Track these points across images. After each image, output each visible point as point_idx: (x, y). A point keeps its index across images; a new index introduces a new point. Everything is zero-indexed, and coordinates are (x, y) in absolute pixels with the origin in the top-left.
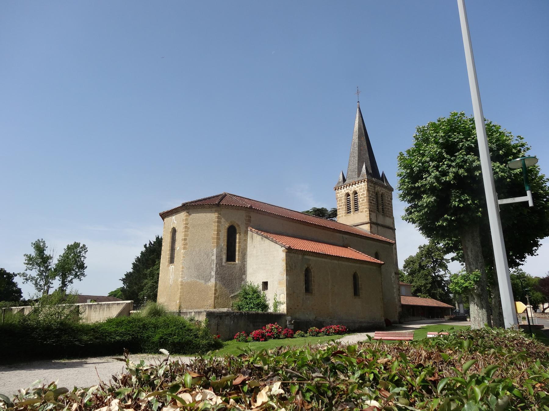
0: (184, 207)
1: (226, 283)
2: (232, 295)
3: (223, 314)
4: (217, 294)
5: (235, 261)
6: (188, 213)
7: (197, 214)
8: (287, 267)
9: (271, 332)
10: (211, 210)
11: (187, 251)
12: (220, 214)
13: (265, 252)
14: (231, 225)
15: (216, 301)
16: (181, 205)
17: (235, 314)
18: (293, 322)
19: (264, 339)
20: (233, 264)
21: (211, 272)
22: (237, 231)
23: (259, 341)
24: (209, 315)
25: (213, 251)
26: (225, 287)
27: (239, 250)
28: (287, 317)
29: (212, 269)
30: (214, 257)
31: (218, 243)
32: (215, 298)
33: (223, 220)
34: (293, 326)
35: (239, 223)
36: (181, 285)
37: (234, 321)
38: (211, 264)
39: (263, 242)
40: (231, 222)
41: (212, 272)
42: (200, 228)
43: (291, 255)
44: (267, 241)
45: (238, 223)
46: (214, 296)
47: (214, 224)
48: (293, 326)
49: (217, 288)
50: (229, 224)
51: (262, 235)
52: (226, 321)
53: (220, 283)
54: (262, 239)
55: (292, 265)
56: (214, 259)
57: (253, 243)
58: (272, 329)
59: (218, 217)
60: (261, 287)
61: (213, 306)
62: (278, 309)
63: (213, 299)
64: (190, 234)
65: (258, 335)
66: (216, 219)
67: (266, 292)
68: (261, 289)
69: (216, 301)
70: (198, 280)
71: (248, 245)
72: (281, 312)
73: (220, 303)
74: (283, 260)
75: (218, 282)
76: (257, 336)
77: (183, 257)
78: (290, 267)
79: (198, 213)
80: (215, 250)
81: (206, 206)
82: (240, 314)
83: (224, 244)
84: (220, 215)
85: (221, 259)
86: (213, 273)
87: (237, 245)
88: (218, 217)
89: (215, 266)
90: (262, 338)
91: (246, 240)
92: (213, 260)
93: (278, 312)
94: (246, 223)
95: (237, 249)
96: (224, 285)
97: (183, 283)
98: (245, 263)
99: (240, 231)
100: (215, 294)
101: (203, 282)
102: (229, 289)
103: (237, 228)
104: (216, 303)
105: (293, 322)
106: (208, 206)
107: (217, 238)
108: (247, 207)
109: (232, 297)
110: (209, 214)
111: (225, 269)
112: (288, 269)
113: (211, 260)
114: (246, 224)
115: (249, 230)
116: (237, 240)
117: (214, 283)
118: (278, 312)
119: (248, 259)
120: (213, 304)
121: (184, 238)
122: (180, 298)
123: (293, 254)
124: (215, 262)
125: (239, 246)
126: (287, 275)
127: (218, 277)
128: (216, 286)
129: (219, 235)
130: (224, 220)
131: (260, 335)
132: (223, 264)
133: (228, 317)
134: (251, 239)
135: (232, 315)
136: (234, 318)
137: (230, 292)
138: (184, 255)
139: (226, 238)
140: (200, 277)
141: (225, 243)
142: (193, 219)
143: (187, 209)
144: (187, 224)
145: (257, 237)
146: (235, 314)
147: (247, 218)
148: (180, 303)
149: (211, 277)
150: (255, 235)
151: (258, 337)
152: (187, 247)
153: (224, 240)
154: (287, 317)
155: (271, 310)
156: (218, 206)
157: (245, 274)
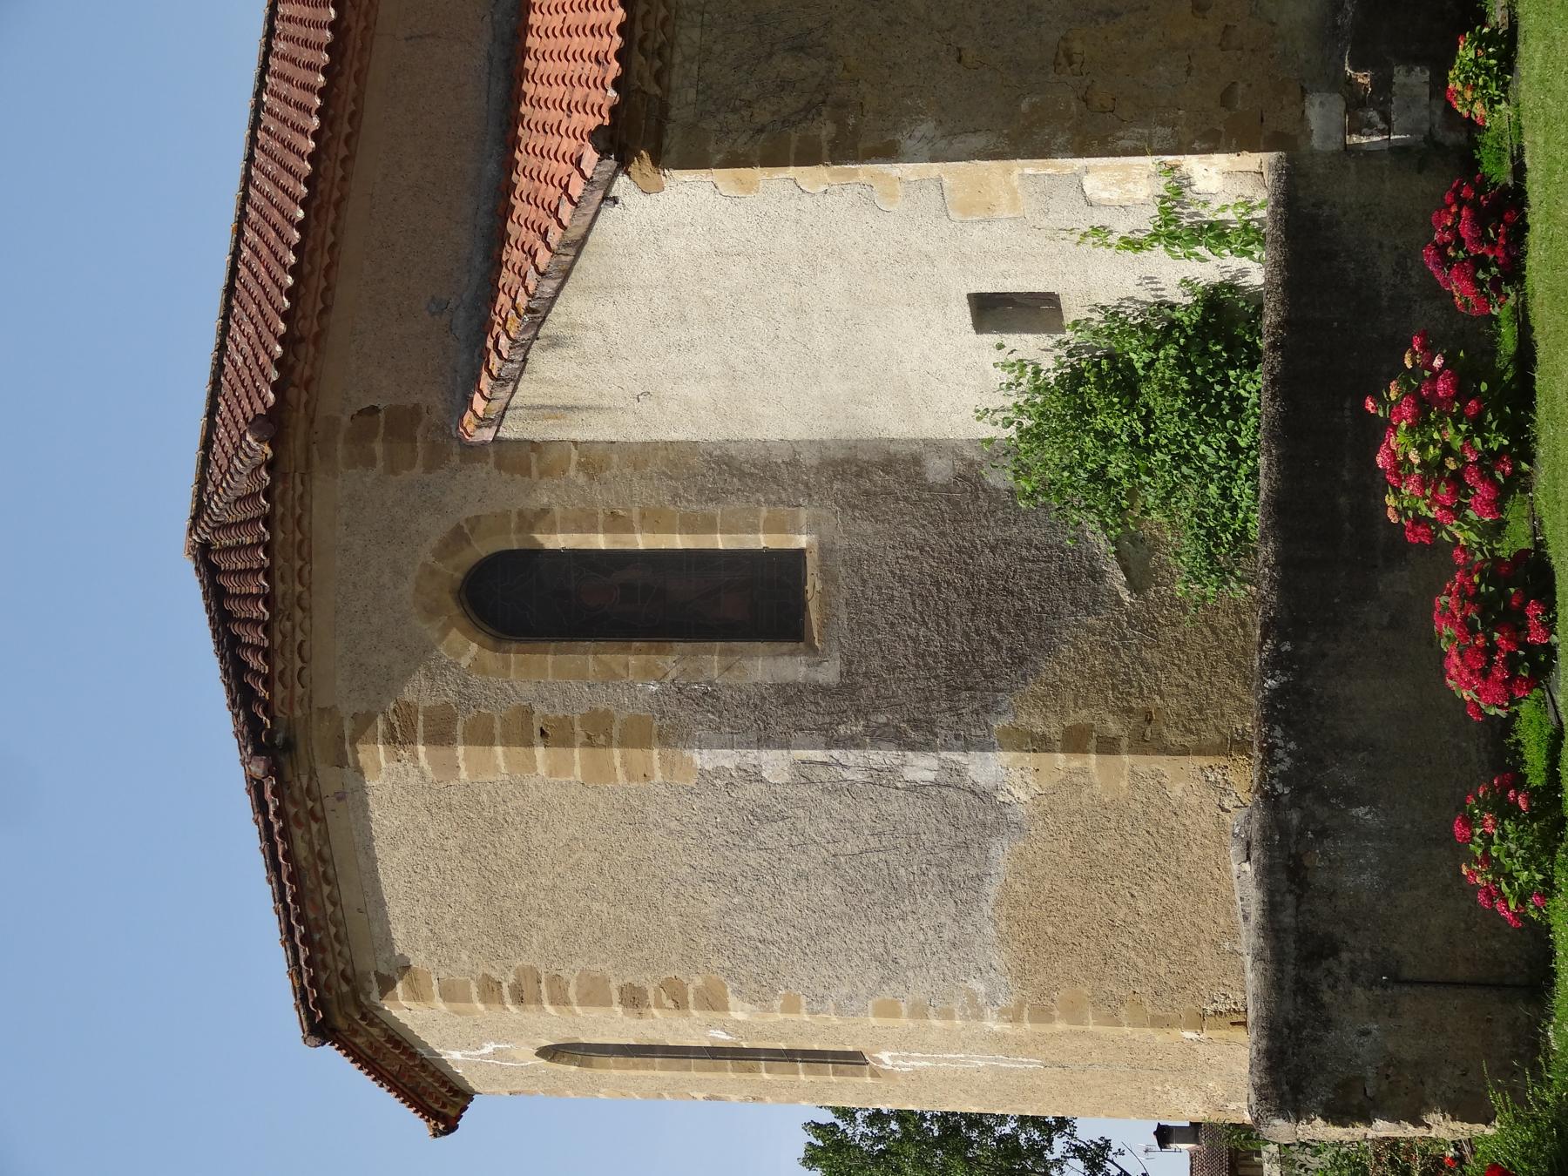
0: (341, 1023)
1: (1006, 643)
2: (1117, 579)
3: (1287, 918)
4: (1113, 727)
5: (800, 553)
6: (387, 985)
7: (394, 910)
8: (808, 156)
9: (1457, 479)
10: (341, 797)
11: (728, 983)
12: (364, 723)
13: (683, 318)
14: (456, 611)
15: (1173, 737)
16: (330, 1052)
17: (1285, 778)
18: (1363, 79)
19: (1534, 610)
20: (828, 576)
21: (914, 787)
22: (514, 543)
23: (1551, 650)
24: (1297, 1089)
25: (719, 772)
26: (1049, 649)
27: (689, 526)
28: (1316, 142)
29: (880, 778)
30: (775, 764)
31: (638, 735)
32: (1145, 743)
33: (418, 692)
34: (1400, 76)
35: (435, 528)
36: (1042, 1014)
37: (1352, 798)
38: (834, 789)
39: (592, 340)
40: (431, 612)
41: (911, 774)
42: (520, 886)
43: (684, 101)
44: (571, 308)
45: (434, 541)
46: (1127, 759)
47: (464, 775)
48: (1400, 76)
49: (1054, 730)
50: (455, 635)
51: (524, 347)
52: (1349, 881)
53: (1006, 700)
54: (555, 343)
55: (784, 85)
56: (785, 765)
57: (606, 402)
58: (1432, 469)
59: (391, 739)
60: (1032, 346)
61: (1223, 761)
62: (1229, 215)
63: (1162, 763)
64: (579, 963)
65: (1490, 662)
66: (415, 757)
67: (1073, 310)
68: (1046, 340)
69: (1173, 737)
70: (992, 889)
71: (638, 435)
72: (1262, 196)
73: (1188, 692)
74: (749, 187)
75: (1003, 722)
76: (1500, 673)
77: (791, 1006)
78: (810, 110)
79: (382, 904)
80: (703, 759)
81: (302, 850)
82: (1288, 724)
83: (647, 673)
84: (369, 719)
85: (790, 695)
86: (922, 767)
87: (641, 541)
88: (399, 737)
89: (852, 756)
90: (1514, 622)
91: (594, 459)
92: (804, 776)
93: (1261, 213)
94: (429, 469)
95: (679, 542)
96: (1023, 660)
97: (1021, 1005)
98: (809, 458)
99: (506, 515)
100: (1108, 746)
101: (1002, 852)
102: (1056, 614)
103: (483, 548)
104: (1190, 740)
105: (1363, 79)
106: (297, 832)
107: (590, 742)
108: (270, 466)
109: (1135, 586)
110: (376, 814)
111: (876, 662)
112: (826, 131)
113: (805, 792)
114: (437, 457)
115: (488, 434)
116: (600, 542)
117: (1005, 757)
118: (1261, 213)
119: (772, 433)
120: (1204, 761)
121: (619, 1009)
122: (1158, 1022)
123: (675, 79)
124: (818, 755)
125: (654, 520)
126: (889, 153)
127: (948, 718)
128: (1041, 744)
129: (565, 724)
130: (419, 679)
131: (1491, 649)
132: (829, 673)
133: (1315, 860)
134: (576, 417)
135: (1294, 817)
136: (1323, 798)
137: (1086, 599)
138: (778, 1003)
139: (589, 660)
140: (959, 871)
141: (633, 660)
142: (442, 945)
143: (355, 993)
144: (490, 990)
145: (542, 381)
146: (1285, 778)
147: (378, 448)
148: (1199, 1020)
149: (952, 780)
150: (527, 391)
151: (1512, 662)
152: (699, 981)
153: (610, 676)
154: (1316, 142)
155: (1254, 272)
156: (289, 746)
157: (916, 460)
